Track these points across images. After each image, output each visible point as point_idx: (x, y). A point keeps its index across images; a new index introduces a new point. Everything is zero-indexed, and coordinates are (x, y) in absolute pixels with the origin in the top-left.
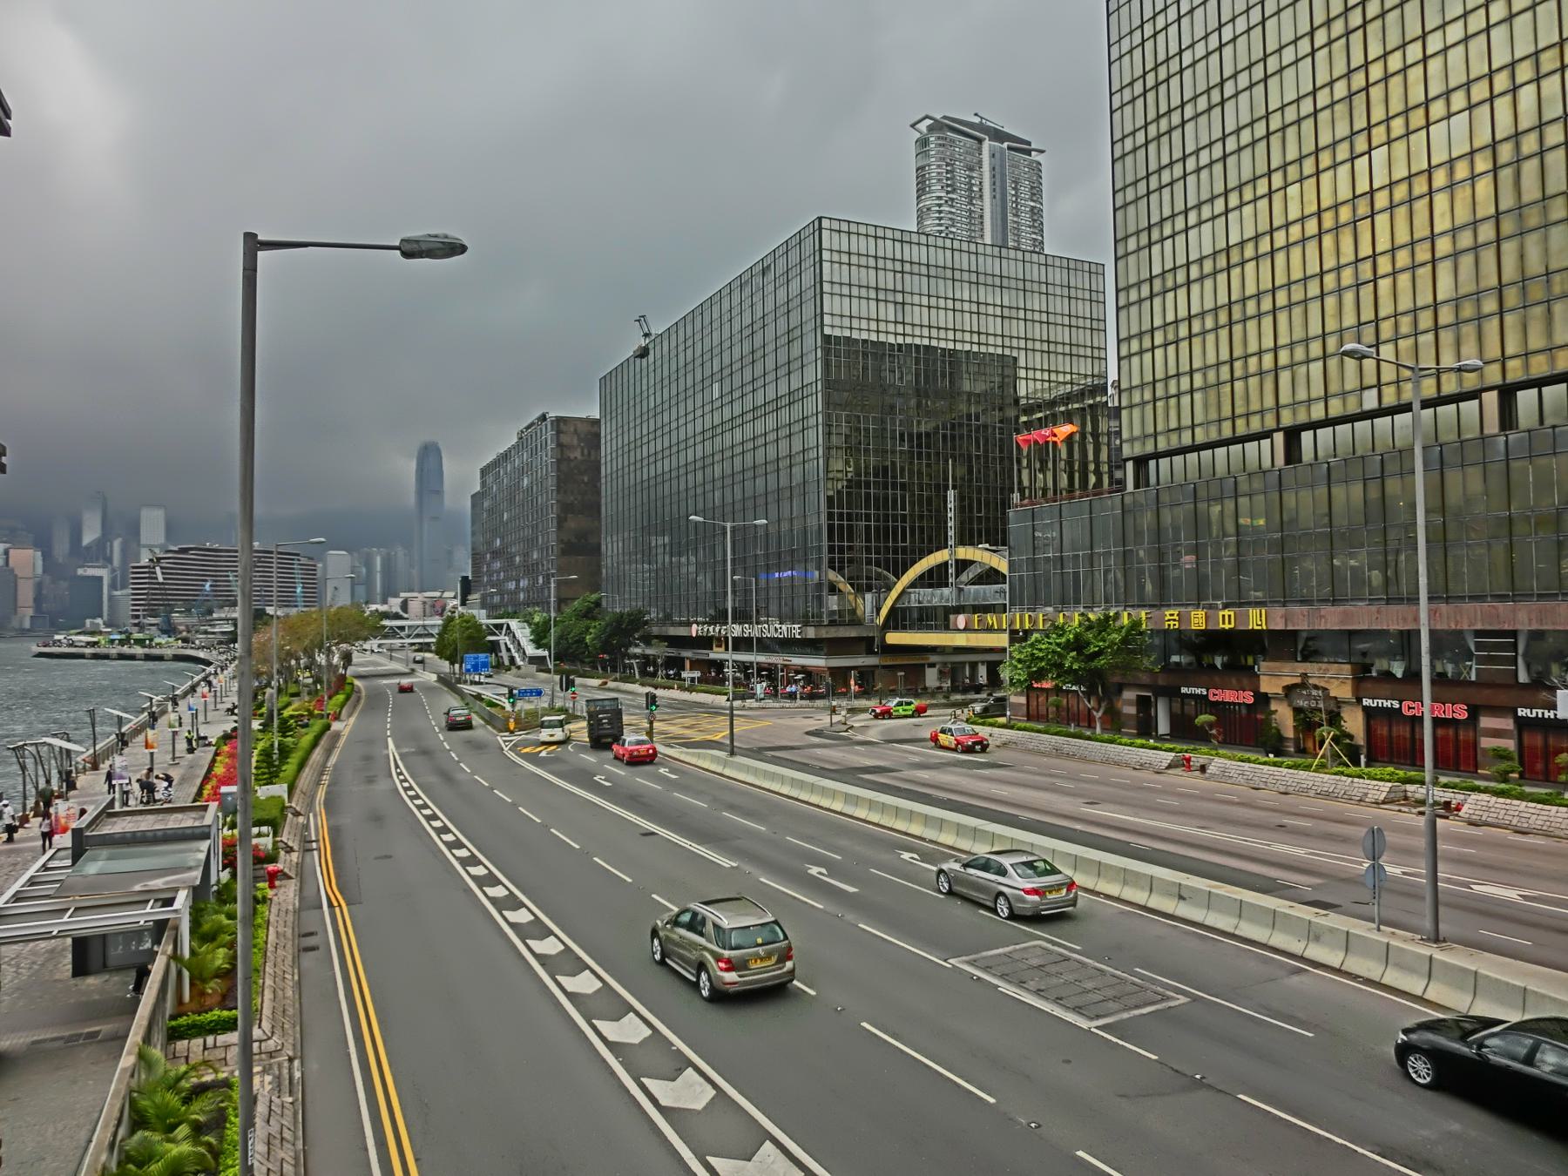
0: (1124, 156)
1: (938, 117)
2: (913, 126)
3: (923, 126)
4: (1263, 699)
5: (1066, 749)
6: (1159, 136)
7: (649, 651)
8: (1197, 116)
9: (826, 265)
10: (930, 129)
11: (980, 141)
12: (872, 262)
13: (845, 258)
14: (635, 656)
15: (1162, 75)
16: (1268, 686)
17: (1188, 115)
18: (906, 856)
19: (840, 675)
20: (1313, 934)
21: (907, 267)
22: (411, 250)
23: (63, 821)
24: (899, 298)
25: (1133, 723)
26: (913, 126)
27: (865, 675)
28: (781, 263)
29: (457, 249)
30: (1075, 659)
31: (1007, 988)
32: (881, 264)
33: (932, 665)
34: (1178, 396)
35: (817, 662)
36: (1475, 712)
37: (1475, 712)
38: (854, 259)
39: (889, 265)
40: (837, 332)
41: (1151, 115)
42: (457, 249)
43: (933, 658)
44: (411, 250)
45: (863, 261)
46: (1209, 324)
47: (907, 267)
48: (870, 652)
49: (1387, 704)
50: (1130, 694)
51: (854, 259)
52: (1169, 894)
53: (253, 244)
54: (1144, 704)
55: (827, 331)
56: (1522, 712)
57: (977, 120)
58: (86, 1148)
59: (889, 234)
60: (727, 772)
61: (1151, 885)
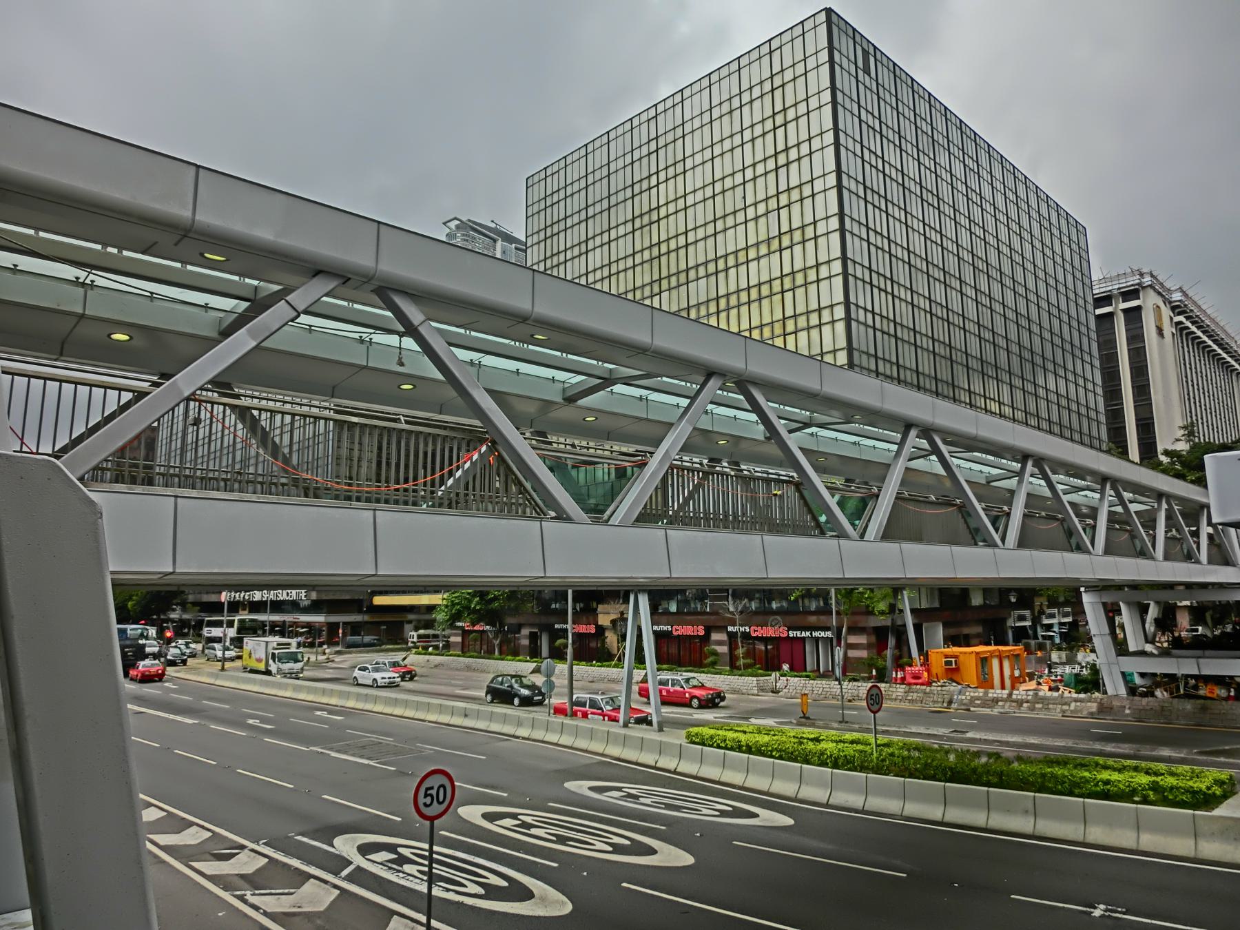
1: (464, 219)
2: (445, 224)
3: (453, 224)
4: (601, 630)
5: (474, 666)
7: (185, 616)
8: (574, 258)
10: (458, 227)
11: (495, 241)
14: (173, 621)
16: (604, 620)
18: (319, 713)
19: (333, 627)
20: (520, 723)
25: (527, 650)
26: (445, 224)
27: (355, 628)
30: (478, 603)
31: (334, 754)
33: (410, 622)
35: (318, 618)
36: (708, 630)
37: (708, 630)
41: (549, 254)
43: (411, 617)
48: (360, 611)
49: (665, 628)
50: (525, 632)
52: (460, 715)
54: (534, 637)
56: (730, 629)
57: (493, 225)
60: (218, 682)
61: (453, 712)
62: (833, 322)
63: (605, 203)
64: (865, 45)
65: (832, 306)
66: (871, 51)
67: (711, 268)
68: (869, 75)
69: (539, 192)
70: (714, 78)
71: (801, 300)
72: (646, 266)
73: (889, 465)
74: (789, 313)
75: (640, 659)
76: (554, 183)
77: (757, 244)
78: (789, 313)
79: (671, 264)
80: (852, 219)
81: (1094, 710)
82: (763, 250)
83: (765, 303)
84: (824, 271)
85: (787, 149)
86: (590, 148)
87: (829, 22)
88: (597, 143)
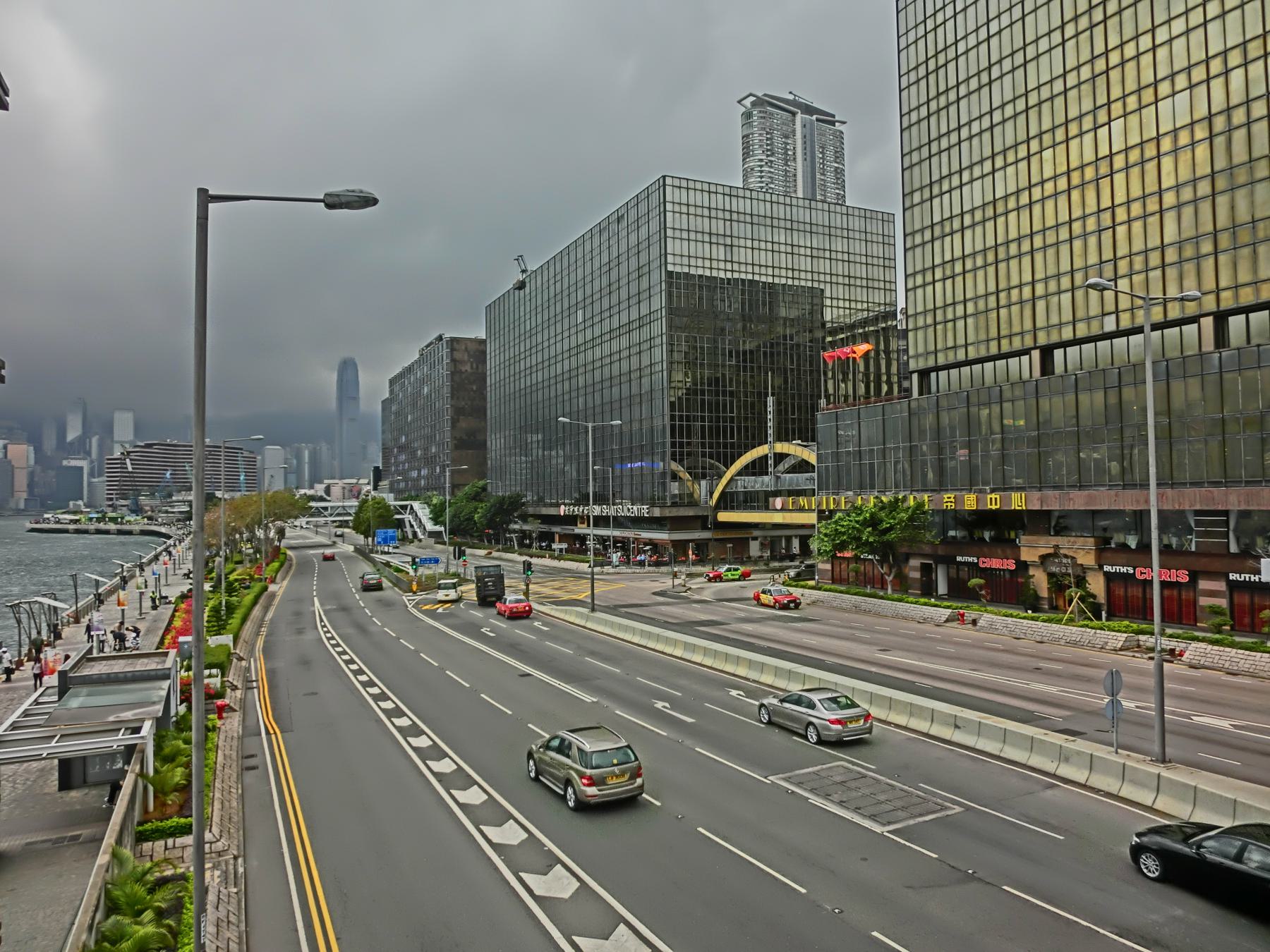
0: (910, 126)
1: (760, 94)
2: (739, 102)
3: (748, 102)
4: (1023, 566)
5: (864, 606)
6: (939, 110)
7: (526, 527)
8: (970, 94)
9: (669, 215)
10: (754, 104)
11: (794, 114)
12: (706, 212)
13: (684, 209)
14: (514, 531)
15: (941, 61)
16: (1027, 555)
17: (962, 93)
18: (734, 693)
19: (680, 546)
20: (1064, 756)
21: (735, 216)
22: (333, 202)
23: (51, 665)
24: (728, 241)
25: (918, 585)
26: (739, 102)
27: (701, 547)
28: (633, 213)
29: (370, 201)
30: (871, 534)
31: (815, 800)
32: (713, 213)
33: (755, 539)
34: (954, 320)
35: (661, 536)
36: (1194, 576)
37: (1194, 576)
38: (692, 210)
39: (720, 214)
40: (678, 269)
41: (933, 93)
42: (370, 201)
43: (756, 533)
44: (333, 202)
45: (699, 211)
46: (979, 262)
47: (735, 216)
48: (705, 528)
49: (1124, 570)
50: (915, 562)
51: (692, 210)
52: (947, 724)
53: (205, 198)
54: (926, 570)
55: (670, 268)
56: (1233, 576)
57: (791, 97)
58: (70, 930)
59: (720, 189)
60: (589, 625)
61: (933, 716)
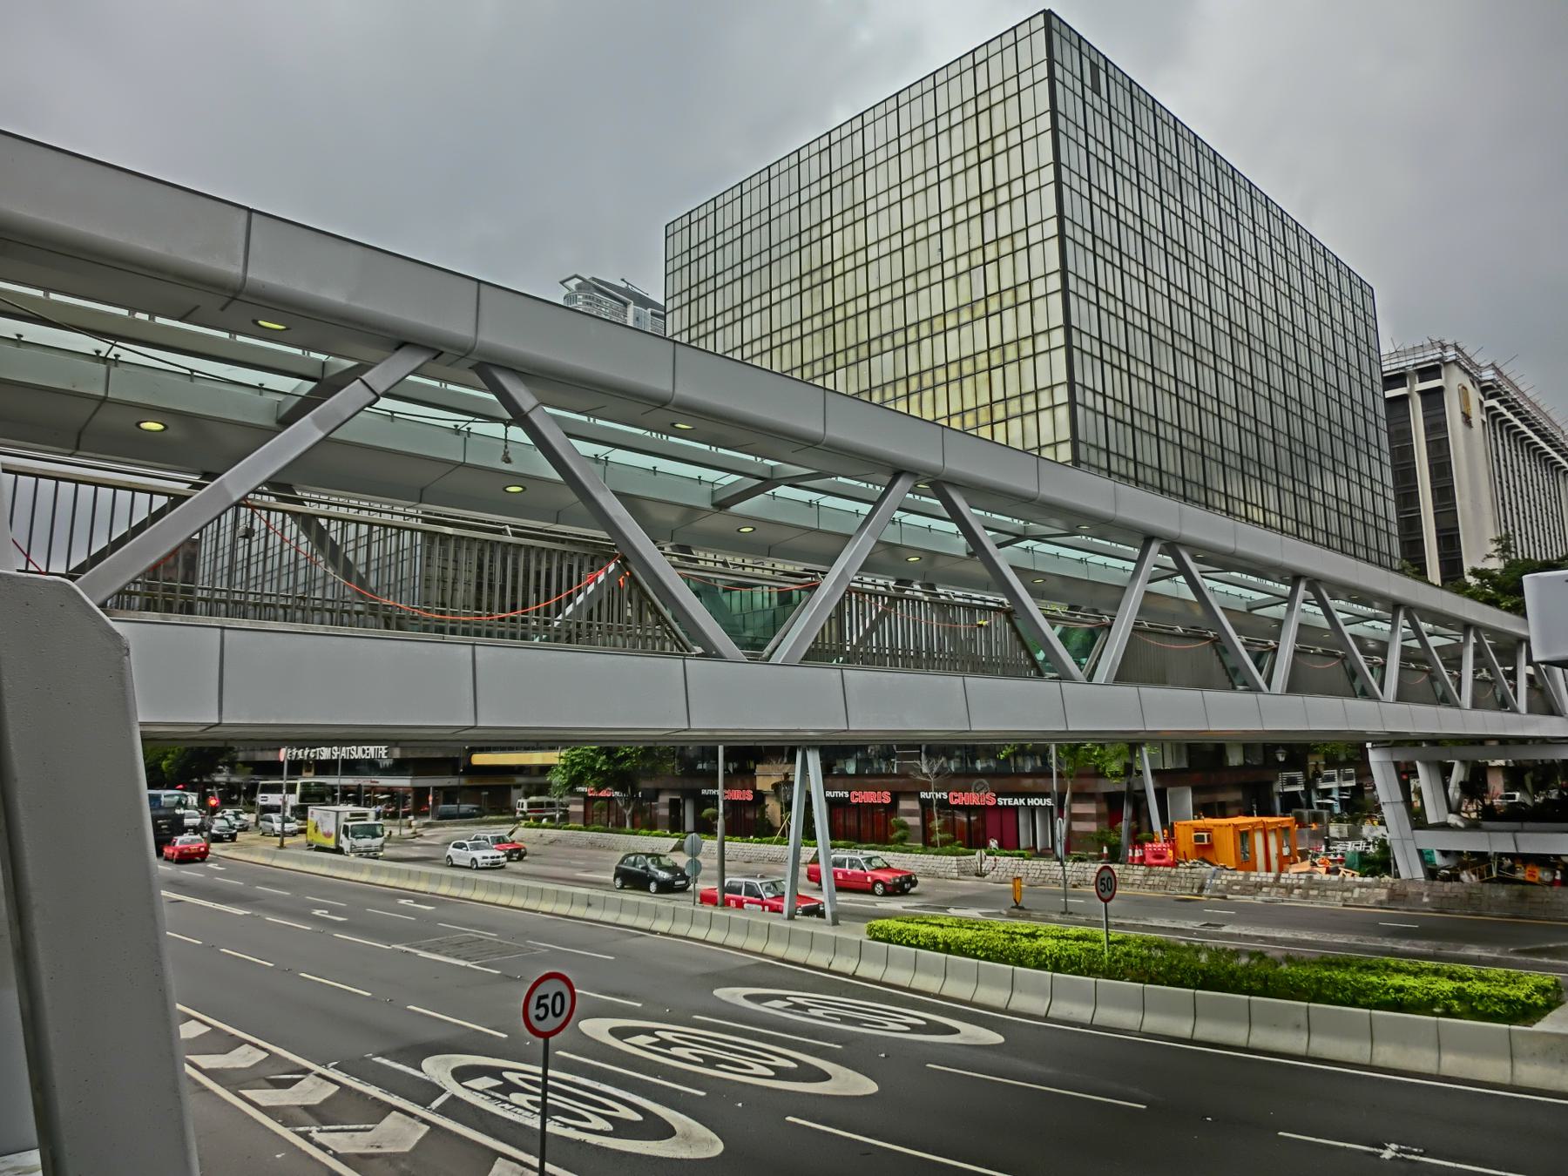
1: (587, 277)
2: (562, 283)
3: (573, 284)
4: (760, 797)
5: (599, 842)
7: (235, 779)
8: (725, 326)
10: (579, 287)
11: (626, 304)
14: (218, 785)
16: (764, 784)
18: (403, 902)
19: (421, 793)
20: (657, 915)
25: (667, 823)
26: (562, 283)
27: (449, 795)
30: (604, 763)
31: (422, 954)
33: (518, 786)
35: (403, 782)
36: (896, 797)
37: (896, 797)
41: (694, 321)
43: (520, 780)
48: (455, 773)
49: (841, 794)
50: (664, 799)
52: (581, 904)
54: (675, 806)
56: (923, 795)
57: (624, 285)
60: (275, 863)
61: (572, 900)
62: (1053, 407)
63: (765, 256)
64: (1094, 57)
65: (1052, 387)
66: (1102, 64)
67: (900, 339)
68: (1099, 95)
69: (681, 242)
70: (903, 98)
71: (1013, 380)
72: (817, 336)
73: (1124, 589)
74: (998, 395)
75: (809, 833)
76: (701, 232)
77: (958, 309)
78: (998, 395)
79: (849, 334)
80: (1078, 277)
81: (1383, 897)
82: (965, 316)
83: (968, 383)
84: (1042, 343)
85: (995, 189)
86: (746, 187)
87: (1048, 27)
88: (755, 181)
